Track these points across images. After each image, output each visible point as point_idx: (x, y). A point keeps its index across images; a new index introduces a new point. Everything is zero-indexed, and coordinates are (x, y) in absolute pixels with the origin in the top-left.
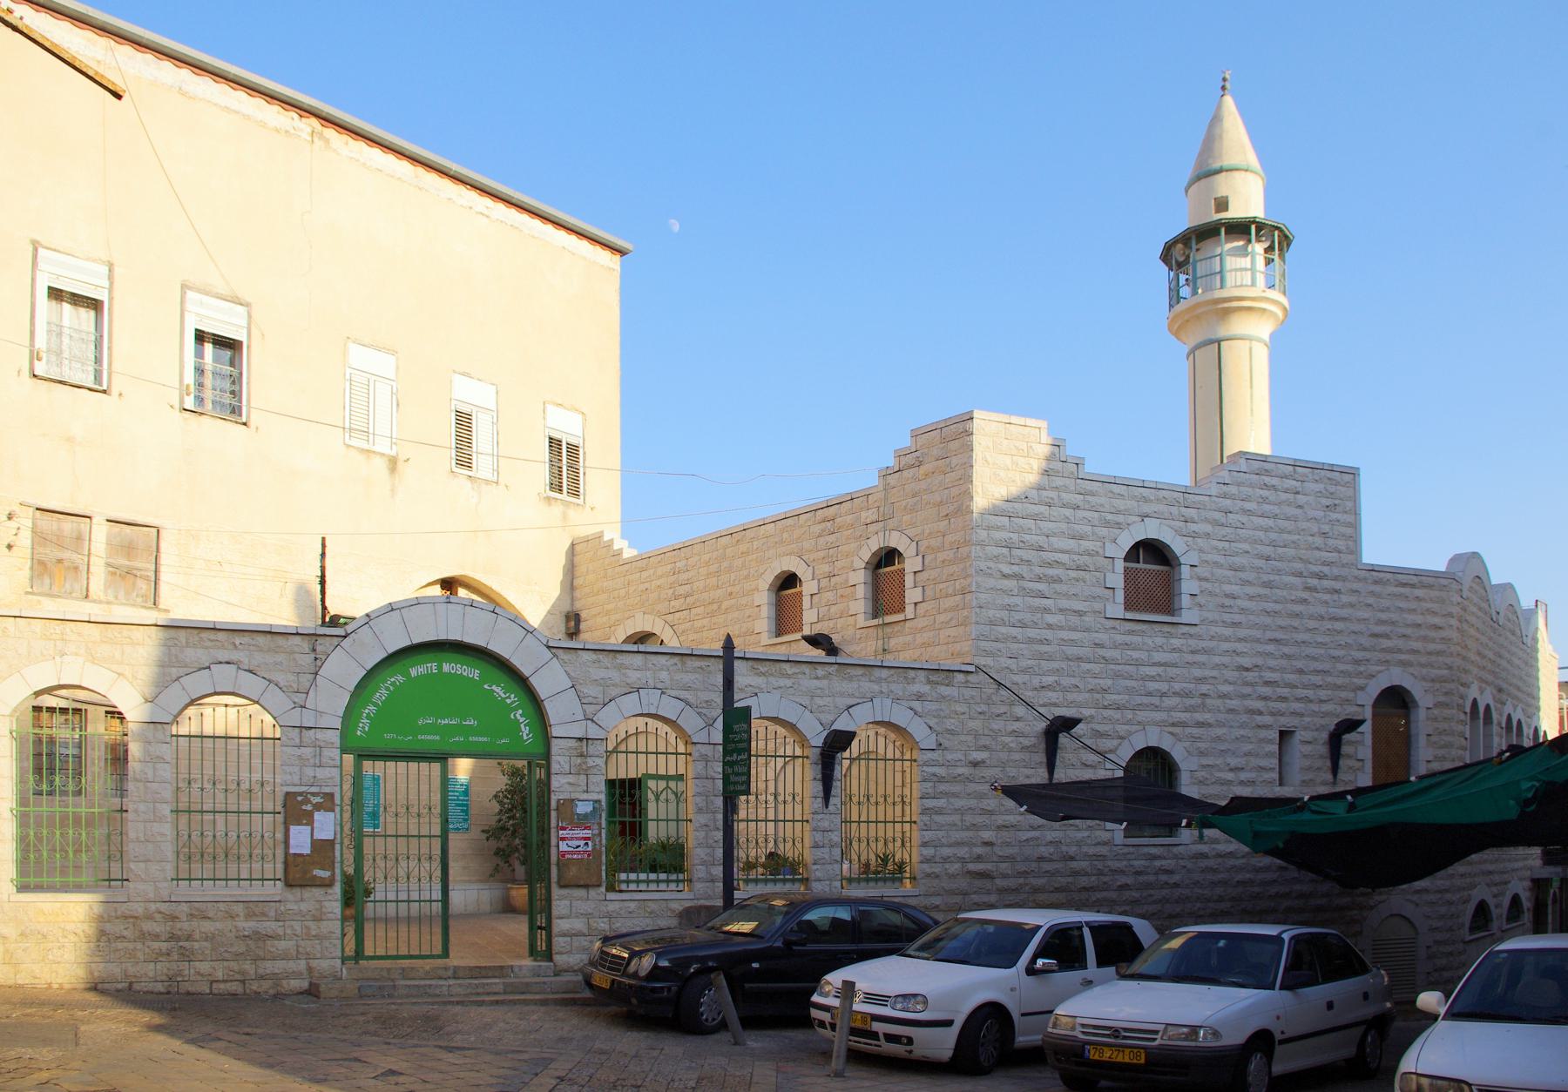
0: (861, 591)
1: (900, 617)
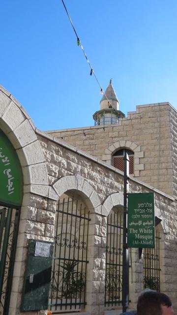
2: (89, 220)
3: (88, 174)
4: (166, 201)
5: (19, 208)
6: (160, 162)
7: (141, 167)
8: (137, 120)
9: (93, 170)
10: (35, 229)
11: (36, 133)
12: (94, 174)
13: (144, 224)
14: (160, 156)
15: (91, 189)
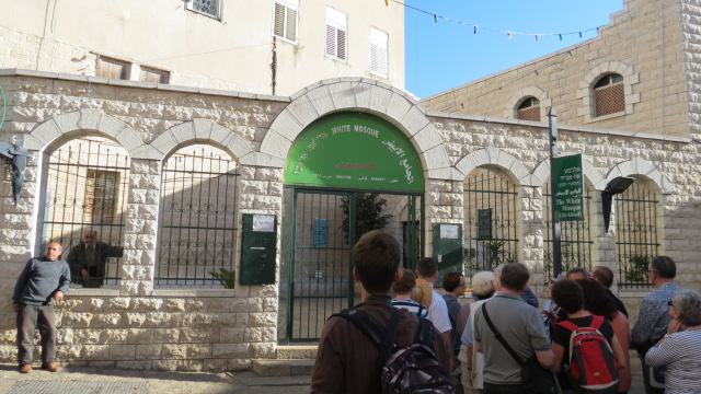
0: (587, 101)
1: (622, 113)
2: (515, 194)
3: (506, 141)
4: (669, 146)
5: (422, 195)
6: (665, 85)
7: (636, 98)
8: (625, 25)
9: (513, 136)
10: (440, 213)
11: (427, 116)
12: (515, 140)
13: (572, 193)
14: (665, 75)
15: (512, 159)
